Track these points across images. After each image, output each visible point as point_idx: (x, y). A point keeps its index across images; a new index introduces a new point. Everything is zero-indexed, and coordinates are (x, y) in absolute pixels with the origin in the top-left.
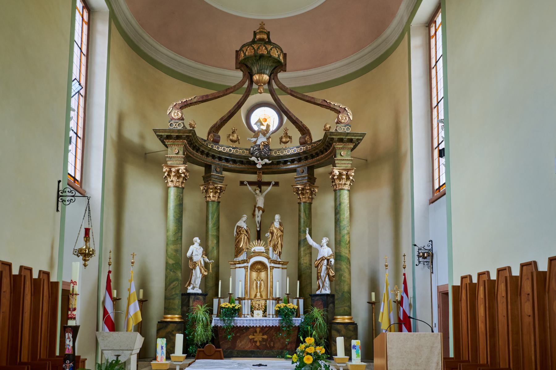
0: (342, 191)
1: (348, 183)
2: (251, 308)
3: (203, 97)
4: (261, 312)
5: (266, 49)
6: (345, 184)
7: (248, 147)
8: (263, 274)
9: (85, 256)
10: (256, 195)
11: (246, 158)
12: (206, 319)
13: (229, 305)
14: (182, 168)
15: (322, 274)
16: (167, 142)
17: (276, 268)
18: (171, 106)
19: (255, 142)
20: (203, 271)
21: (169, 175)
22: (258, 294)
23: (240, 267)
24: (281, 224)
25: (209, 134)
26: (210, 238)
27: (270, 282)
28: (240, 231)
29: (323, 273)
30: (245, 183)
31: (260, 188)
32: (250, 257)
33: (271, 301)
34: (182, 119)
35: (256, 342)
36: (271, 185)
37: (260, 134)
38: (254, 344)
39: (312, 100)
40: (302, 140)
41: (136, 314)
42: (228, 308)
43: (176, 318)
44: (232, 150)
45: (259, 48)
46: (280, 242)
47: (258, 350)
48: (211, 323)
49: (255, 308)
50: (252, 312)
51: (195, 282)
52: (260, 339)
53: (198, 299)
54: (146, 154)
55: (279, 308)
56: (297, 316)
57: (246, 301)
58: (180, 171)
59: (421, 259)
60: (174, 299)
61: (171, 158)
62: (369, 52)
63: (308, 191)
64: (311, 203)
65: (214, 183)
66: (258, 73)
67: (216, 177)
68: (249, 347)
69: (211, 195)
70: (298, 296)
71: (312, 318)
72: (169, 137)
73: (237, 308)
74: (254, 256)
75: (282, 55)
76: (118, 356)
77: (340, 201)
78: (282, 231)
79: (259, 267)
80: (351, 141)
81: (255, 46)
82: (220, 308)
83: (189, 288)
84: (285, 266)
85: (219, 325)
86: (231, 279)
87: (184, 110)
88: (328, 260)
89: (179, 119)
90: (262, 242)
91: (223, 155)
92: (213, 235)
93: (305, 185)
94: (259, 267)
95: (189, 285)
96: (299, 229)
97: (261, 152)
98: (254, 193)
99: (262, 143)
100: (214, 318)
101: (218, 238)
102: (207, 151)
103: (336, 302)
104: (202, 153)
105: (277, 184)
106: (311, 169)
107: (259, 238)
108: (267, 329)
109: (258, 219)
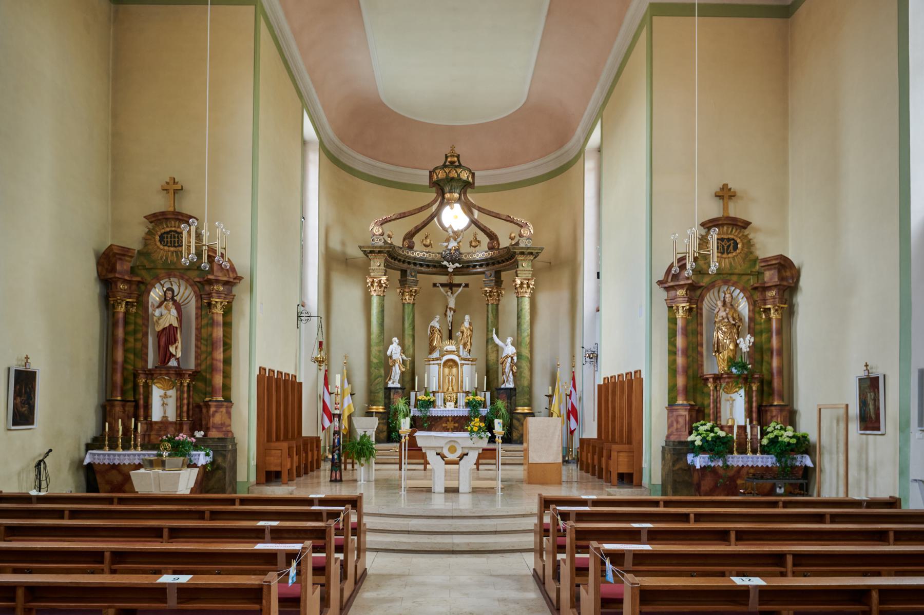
0: (523, 298)
1: (529, 291)
2: (444, 400)
3: (400, 214)
4: (452, 404)
5: (456, 172)
6: (526, 292)
8: (454, 370)
9: (320, 363)
10: (447, 297)
11: (439, 262)
12: (406, 410)
13: (425, 398)
14: (383, 279)
15: (506, 371)
16: (371, 256)
17: (466, 364)
18: (373, 223)
19: (447, 246)
20: (401, 367)
21: (372, 285)
22: (450, 388)
23: (434, 364)
24: (470, 324)
25: (404, 240)
27: (461, 377)
28: (433, 331)
29: (507, 370)
30: (438, 285)
31: (452, 290)
32: (443, 356)
33: (462, 394)
34: (382, 234)
37: (452, 239)
39: (498, 216)
40: (490, 245)
41: (349, 406)
42: (424, 400)
43: (380, 409)
44: (426, 254)
45: (450, 172)
46: (470, 340)
48: (410, 413)
49: (448, 400)
50: (445, 403)
51: (395, 377)
52: (452, 427)
53: (397, 392)
54: (347, 259)
55: (469, 400)
56: (484, 407)
57: (439, 394)
58: (382, 282)
59: (588, 359)
60: (378, 393)
61: (373, 270)
62: (552, 160)
63: (495, 294)
64: (497, 305)
65: (409, 287)
66: (449, 192)
67: (411, 281)
69: (407, 297)
70: (485, 390)
71: (496, 409)
72: (371, 252)
73: (432, 400)
74: (447, 354)
75: (470, 176)
76: (365, 432)
77: (521, 307)
78: (471, 331)
79: (451, 364)
80: (531, 254)
81: (447, 170)
82: (417, 400)
83: (390, 383)
84: (474, 363)
86: (426, 375)
87: (384, 226)
88: (512, 358)
89: (380, 235)
90: (453, 342)
91: (418, 261)
92: (409, 335)
93: (492, 288)
94: (451, 364)
95: (389, 380)
96: (487, 328)
97: (452, 256)
98: (446, 294)
99: (453, 248)
100: (412, 409)
102: (403, 259)
103: (517, 395)
104: (399, 261)
105: (467, 285)
106: (498, 274)
107: (450, 337)
109: (450, 319)
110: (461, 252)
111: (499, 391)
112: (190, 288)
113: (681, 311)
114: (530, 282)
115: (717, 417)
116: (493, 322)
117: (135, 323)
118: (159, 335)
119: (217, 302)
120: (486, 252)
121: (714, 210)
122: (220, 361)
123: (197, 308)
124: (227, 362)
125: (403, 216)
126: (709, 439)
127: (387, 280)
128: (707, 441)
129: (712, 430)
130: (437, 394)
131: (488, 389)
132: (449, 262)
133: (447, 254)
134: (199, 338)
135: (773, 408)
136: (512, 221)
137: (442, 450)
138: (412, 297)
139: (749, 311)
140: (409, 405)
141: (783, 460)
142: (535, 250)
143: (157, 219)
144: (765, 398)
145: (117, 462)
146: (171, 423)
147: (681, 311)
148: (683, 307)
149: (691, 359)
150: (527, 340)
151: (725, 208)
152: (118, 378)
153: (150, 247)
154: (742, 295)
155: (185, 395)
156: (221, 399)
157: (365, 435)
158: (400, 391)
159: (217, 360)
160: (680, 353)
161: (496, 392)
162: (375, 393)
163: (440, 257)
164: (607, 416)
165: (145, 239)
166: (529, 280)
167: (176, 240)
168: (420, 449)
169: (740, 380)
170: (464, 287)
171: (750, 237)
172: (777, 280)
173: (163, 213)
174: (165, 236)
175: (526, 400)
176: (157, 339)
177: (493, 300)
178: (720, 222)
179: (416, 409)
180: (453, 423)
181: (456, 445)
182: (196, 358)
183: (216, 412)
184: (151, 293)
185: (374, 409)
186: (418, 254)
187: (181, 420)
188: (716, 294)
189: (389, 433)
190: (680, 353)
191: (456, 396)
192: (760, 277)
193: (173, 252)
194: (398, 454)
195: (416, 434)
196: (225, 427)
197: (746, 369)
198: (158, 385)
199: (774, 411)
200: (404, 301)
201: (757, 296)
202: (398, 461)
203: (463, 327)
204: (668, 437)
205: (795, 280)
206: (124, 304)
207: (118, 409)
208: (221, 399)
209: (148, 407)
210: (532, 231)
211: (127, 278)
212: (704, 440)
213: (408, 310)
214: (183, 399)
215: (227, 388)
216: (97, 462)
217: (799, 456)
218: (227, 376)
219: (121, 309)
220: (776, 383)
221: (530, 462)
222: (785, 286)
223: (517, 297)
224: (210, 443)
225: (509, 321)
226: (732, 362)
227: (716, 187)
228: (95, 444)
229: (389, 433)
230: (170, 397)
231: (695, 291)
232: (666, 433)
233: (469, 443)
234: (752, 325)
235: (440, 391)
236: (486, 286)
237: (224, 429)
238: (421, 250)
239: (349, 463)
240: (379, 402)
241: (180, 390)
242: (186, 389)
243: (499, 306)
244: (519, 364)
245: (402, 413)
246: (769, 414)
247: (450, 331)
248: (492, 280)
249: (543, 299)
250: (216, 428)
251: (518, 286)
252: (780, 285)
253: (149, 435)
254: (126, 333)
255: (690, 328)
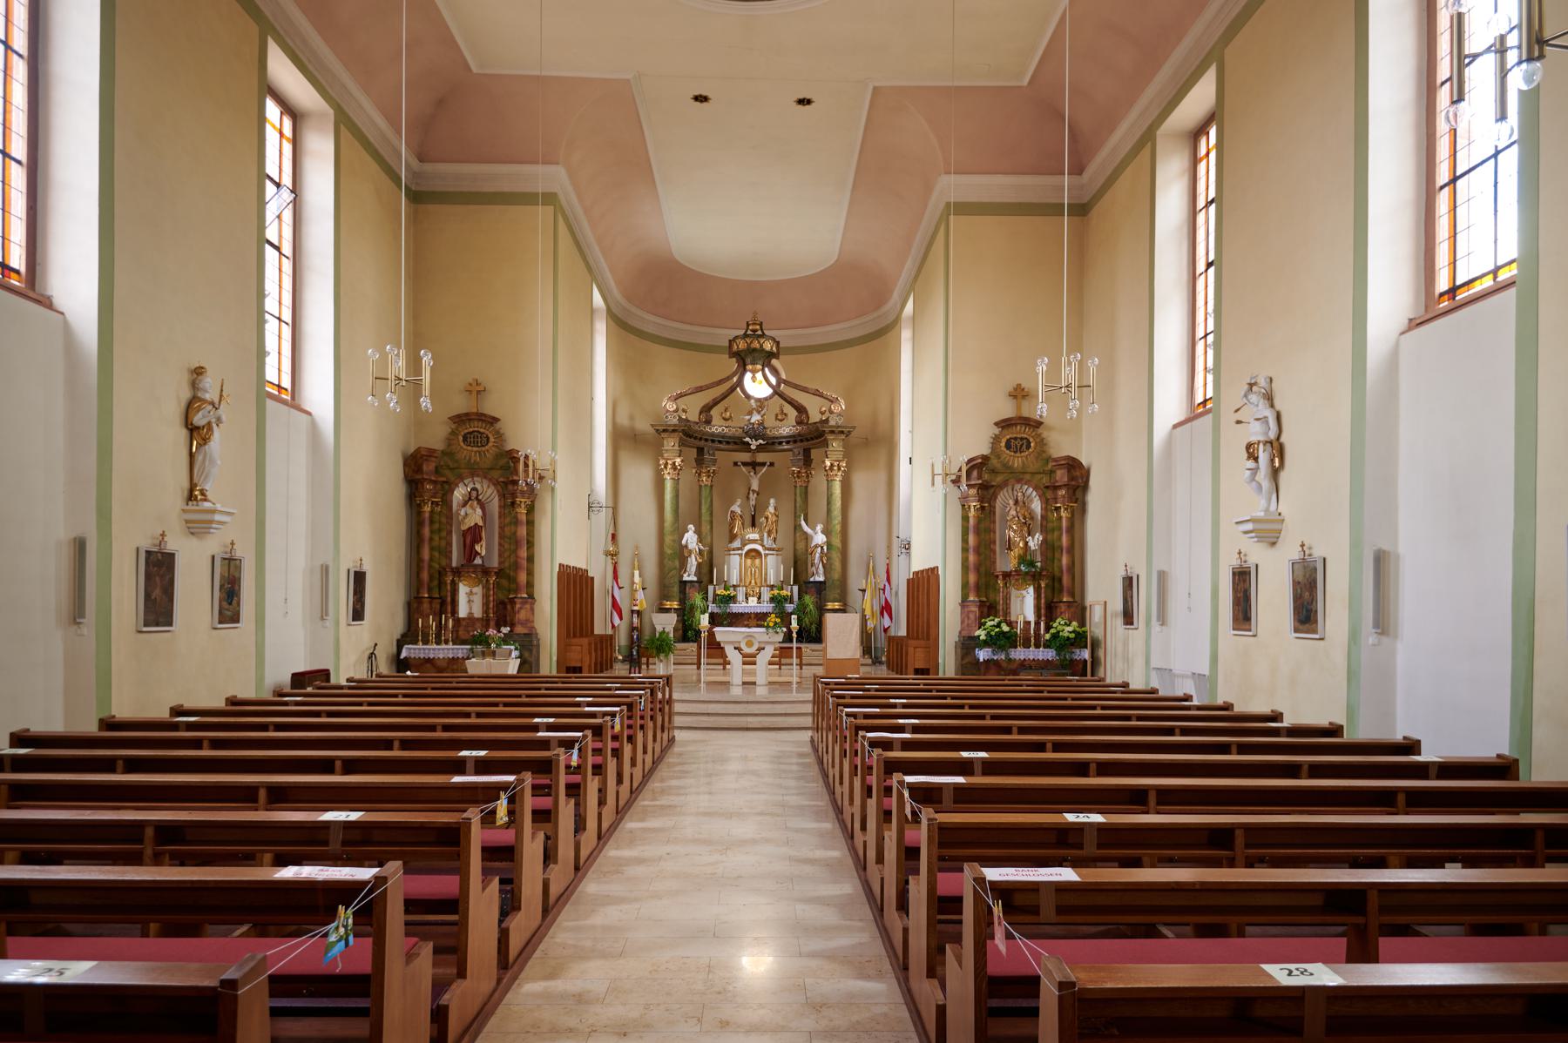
1: (840, 473)
4: (755, 599)
5: (759, 342)
7: (742, 426)
14: (678, 460)
15: (816, 561)
19: (749, 420)
21: (666, 467)
22: (753, 581)
24: (775, 509)
25: (701, 413)
26: (703, 523)
32: (744, 545)
34: (676, 411)
37: (755, 412)
45: (751, 342)
50: (747, 599)
53: (693, 586)
58: (677, 464)
59: (904, 550)
60: (673, 587)
61: (667, 450)
64: (807, 487)
65: (706, 467)
66: (751, 364)
69: (704, 479)
72: (664, 431)
78: (777, 516)
79: (752, 554)
80: (842, 432)
82: (715, 595)
85: (715, 611)
87: (678, 401)
88: (822, 547)
93: (801, 468)
95: (685, 572)
96: (795, 513)
101: (711, 522)
104: (696, 438)
105: (772, 464)
107: (753, 525)
109: (753, 502)
112: (492, 487)
113: (972, 510)
115: (1007, 613)
116: (802, 508)
117: (440, 522)
118: (465, 534)
119: (521, 502)
120: (794, 426)
121: (1007, 410)
122: (524, 559)
123: (500, 507)
124: (531, 559)
125: (699, 389)
126: (993, 633)
128: (991, 636)
129: (998, 625)
131: (795, 583)
134: (501, 537)
135: (1061, 604)
136: (821, 395)
139: (1042, 509)
140: (707, 601)
141: (1063, 653)
143: (460, 419)
144: (1056, 595)
145: (432, 656)
146: (478, 619)
147: (972, 510)
148: (975, 506)
149: (983, 556)
150: (838, 528)
151: (1019, 407)
152: (425, 576)
153: (454, 447)
154: (1034, 493)
155: (492, 592)
156: (526, 596)
157: (664, 631)
159: (521, 558)
160: (971, 551)
164: (913, 613)
165: (448, 439)
166: (839, 461)
167: (479, 440)
168: (719, 644)
169: (1029, 577)
171: (1044, 436)
172: (1066, 480)
173: (467, 414)
174: (468, 436)
175: (837, 596)
176: (462, 540)
178: (1013, 422)
181: (753, 639)
182: (500, 556)
183: (521, 608)
184: (455, 492)
185: (668, 604)
186: (717, 429)
187: (487, 616)
188: (1010, 491)
189: (687, 632)
190: (971, 551)
191: (760, 590)
192: (1052, 475)
193: (476, 452)
194: (695, 654)
195: (715, 629)
196: (528, 622)
197: (1034, 566)
198: (466, 583)
199: (1063, 607)
201: (1049, 494)
202: (695, 661)
204: (960, 633)
205: (1084, 480)
206: (430, 503)
207: (426, 606)
208: (526, 596)
209: (454, 603)
210: (844, 407)
211: (433, 478)
212: (988, 634)
213: (705, 492)
214: (489, 596)
215: (530, 585)
216: (413, 656)
217: (1078, 651)
218: (530, 573)
219: (427, 509)
220: (1066, 580)
222: (1073, 486)
223: (827, 480)
224: (516, 637)
225: (818, 505)
226: (1022, 559)
227: (1010, 388)
228: (408, 637)
229: (687, 632)
230: (476, 594)
231: (987, 493)
232: (959, 629)
233: (765, 638)
234: (1044, 523)
236: (794, 466)
237: (529, 625)
238: (721, 424)
239: (644, 664)
240: (673, 597)
241: (486, 588)
242: (492, 586)
243: (809, 488)
246: (1058, 610)
247: (753, 517)
249: (860, 481)
250: (522, 624)
252: (1068, 485)
253: (457, 631)
254: (432, 532)
255: (982, 526)
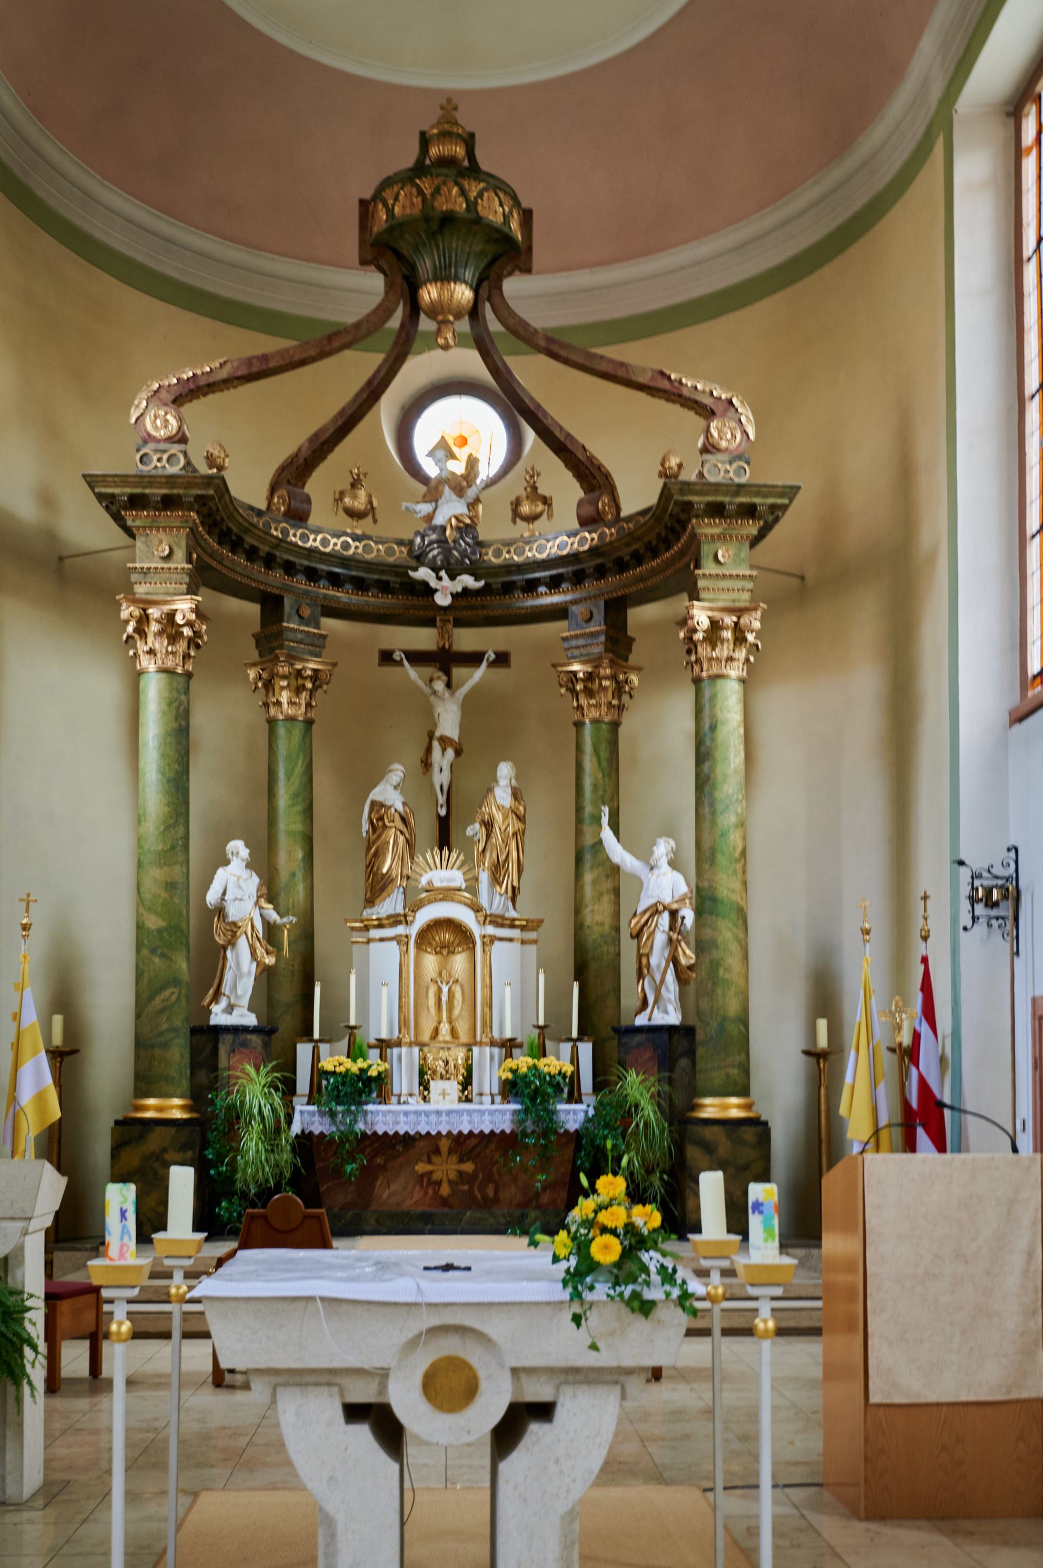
0: (720, 683)
1: (741, 654)
2: (422, 1073)
3: (249, 361)
4: (453, 1087)
6: (730, 659)
7: (407, 536)
8: (459, 962)
10: (432, 698)
11: (400, 571)
12: (273, 1110)
14: (184, 607)
15: (654, 961)
16: (131, 518)
17: (501, 939)
19: (430, 517)
21: (141, 631)
22: (445, 1028)
23: (382, 940)
24: (516, 795)
25: (273, 489)
27: (483, 986)
29: (658, 957)
30: (397, 656)
32: (416, 907)
33: (487, 1049)
35: (439, 1183)
36: (484, 664)
37: (447, 490)
38: (430, 1192)
40: (589, 510)
41: (40, 1098)
43: (172, 1107)
46: (514, 854)
47: (446, 1210)
49: (435, 1072)
50: (425, 1085)
51: (234, 988)
52: (452, 1176)
53: (244, 1044)
55: (514, 1071)
57: (404, 1050)
58: (179, 619)
60: (165, 1046)
61: (145, 572)
64: (615, 725)
65: (292, 658)
67: (299, 636)
68: (414, 1200)
69: (284, 697)
70: (575, 1034)
72: (137, 502)
73: (373, 1073)
74: (430, 902)
75: (515, 215)
78: (521, 819)
80: (750, 511)
81: (426, 185)
82: (318, 1074)
84: (532, 935)
85: (317, 1129)
86: (353, 978)
87: (188, 409)
88: (674, 914)
90: (454, 855)
92: (291, 833)
95: (216, 998)
96: (579, 809)
99: (454, 521)
101: (308, 840)
102: (267, 549)
103: (700, 1051)
104: (252, 554)
105: (502, 659)
107: (444, 840)
108: (473, 1141)
109: (441, 778)
110: (482, 537)
111: (625, 1040)
114: (744, 621)
127: (197, 611)
130: (396, 1051)
132: (436, 570)
133: (431, 543)
136: (675, 395)
137: (383, 1388)
138: (304, 695)
142: (765, 496)
158: (255, 1039)
161: (615, 1043)
162: (152, 1046)
163: (405, 555)
170: (492, 664)
177: (598, 706)
179: (313, 1108)
180: (454, 1158)
186: (325, 542)
200: (273, 711)
203: (490, 805)
221: (874, 1399)
223: (697, 681)
235: (406, 1039)
243: (622, 730)
244: (707, 933)
245: (256, 1126)
248: (593, 635)
251: (699, 636)
